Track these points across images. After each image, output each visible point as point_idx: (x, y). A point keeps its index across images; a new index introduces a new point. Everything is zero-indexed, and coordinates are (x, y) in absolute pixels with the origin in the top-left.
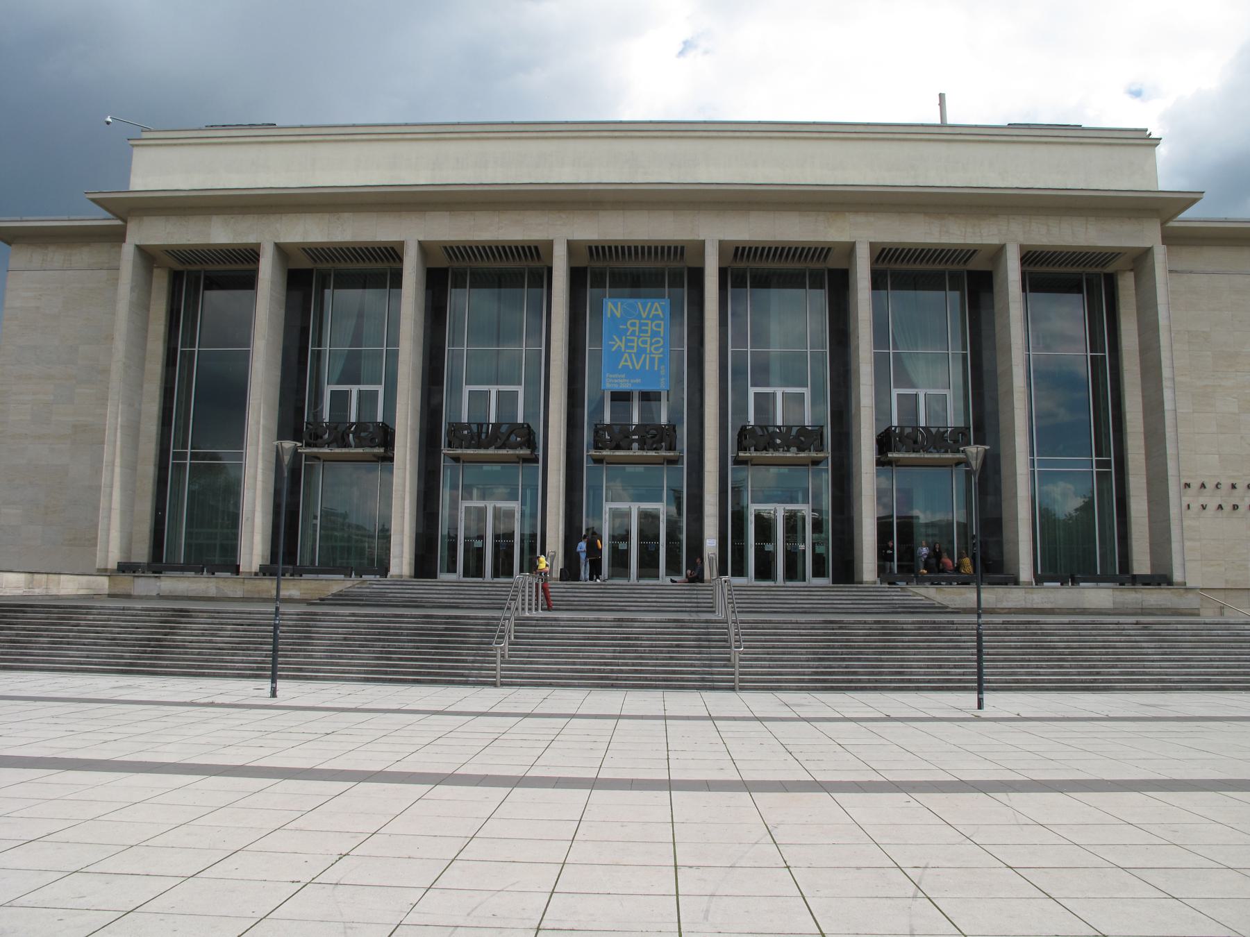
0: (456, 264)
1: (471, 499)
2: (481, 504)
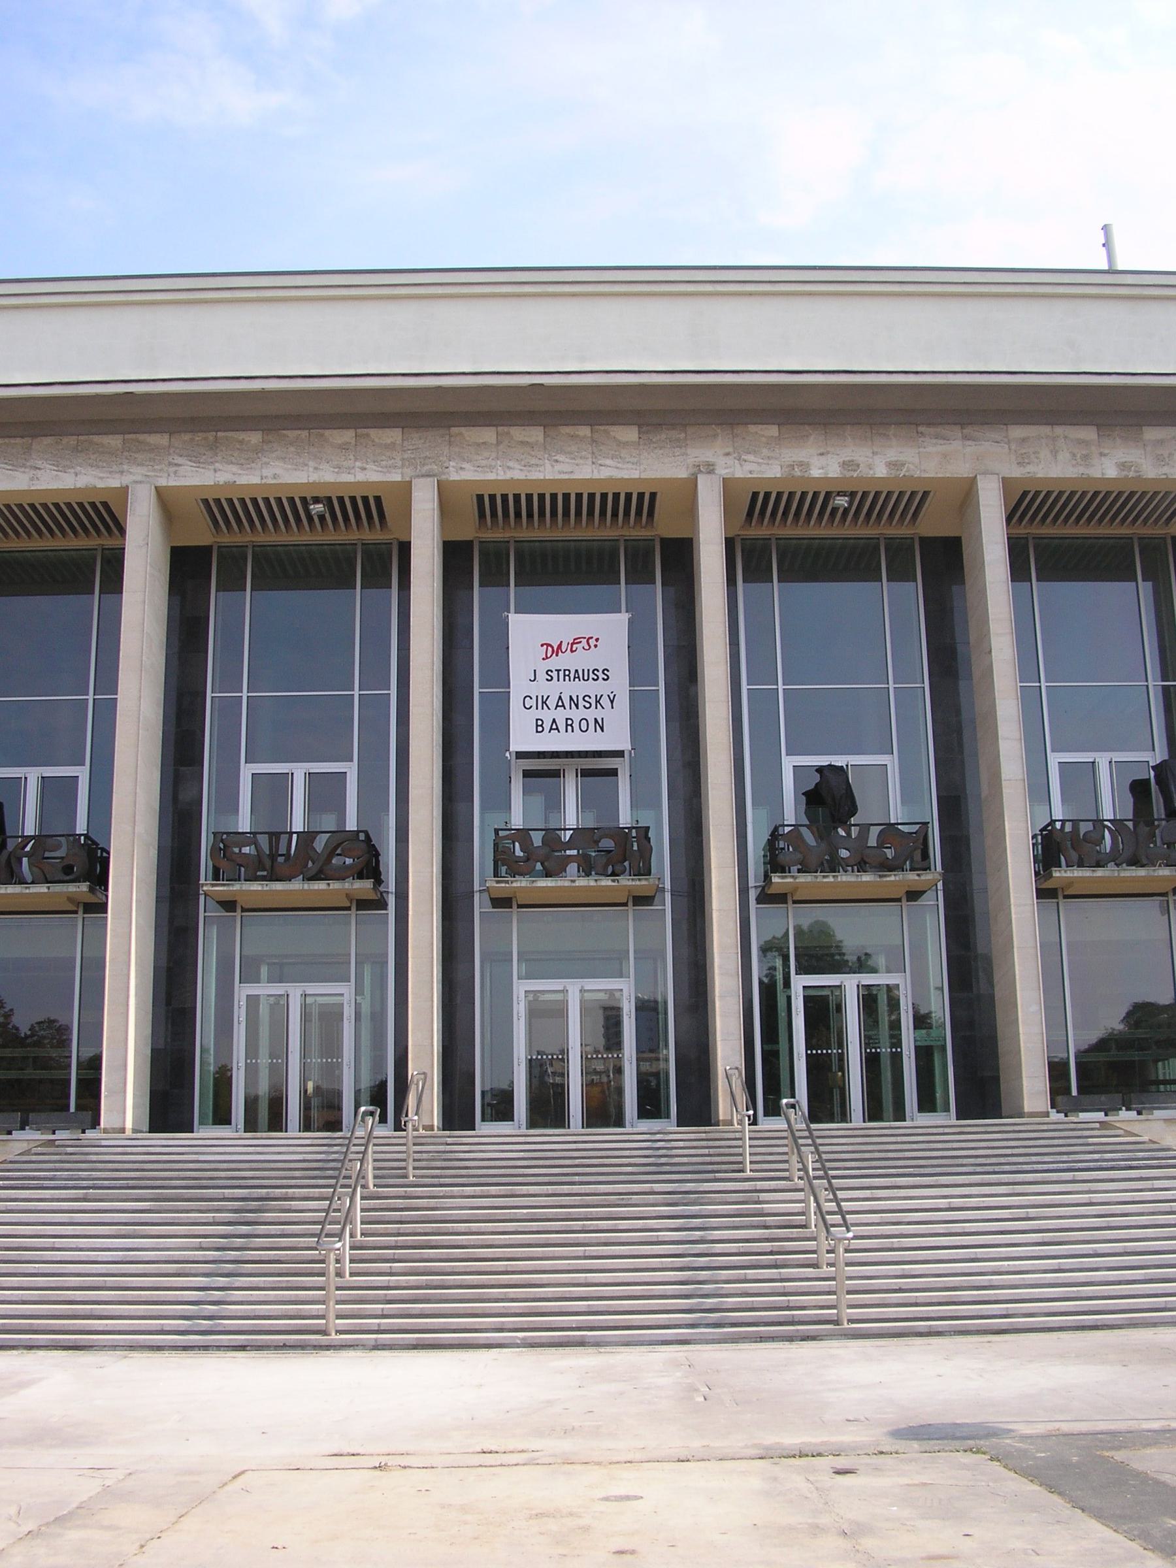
0: (226, 539)
1: (257, 980)
2: (278, 989)
